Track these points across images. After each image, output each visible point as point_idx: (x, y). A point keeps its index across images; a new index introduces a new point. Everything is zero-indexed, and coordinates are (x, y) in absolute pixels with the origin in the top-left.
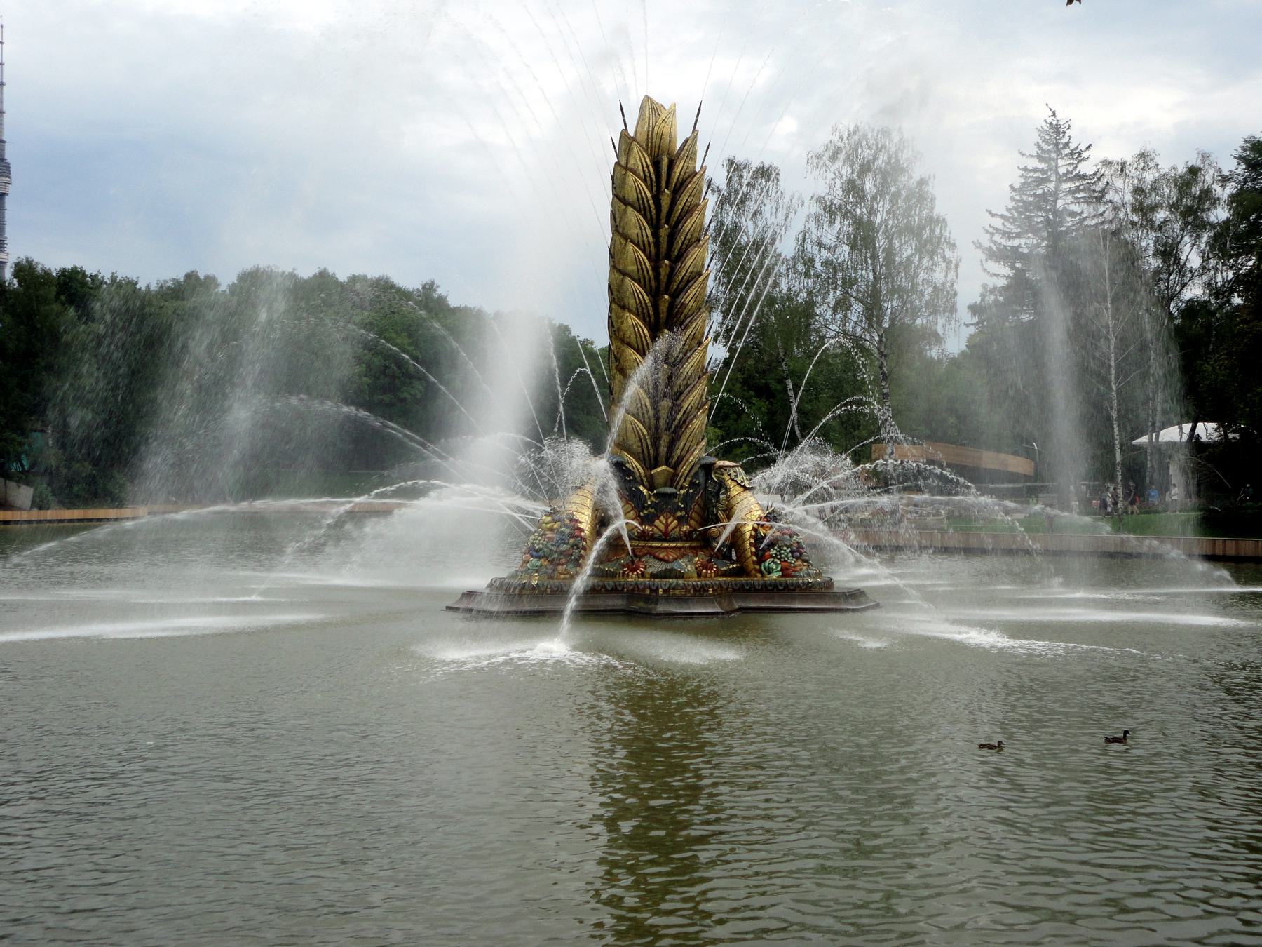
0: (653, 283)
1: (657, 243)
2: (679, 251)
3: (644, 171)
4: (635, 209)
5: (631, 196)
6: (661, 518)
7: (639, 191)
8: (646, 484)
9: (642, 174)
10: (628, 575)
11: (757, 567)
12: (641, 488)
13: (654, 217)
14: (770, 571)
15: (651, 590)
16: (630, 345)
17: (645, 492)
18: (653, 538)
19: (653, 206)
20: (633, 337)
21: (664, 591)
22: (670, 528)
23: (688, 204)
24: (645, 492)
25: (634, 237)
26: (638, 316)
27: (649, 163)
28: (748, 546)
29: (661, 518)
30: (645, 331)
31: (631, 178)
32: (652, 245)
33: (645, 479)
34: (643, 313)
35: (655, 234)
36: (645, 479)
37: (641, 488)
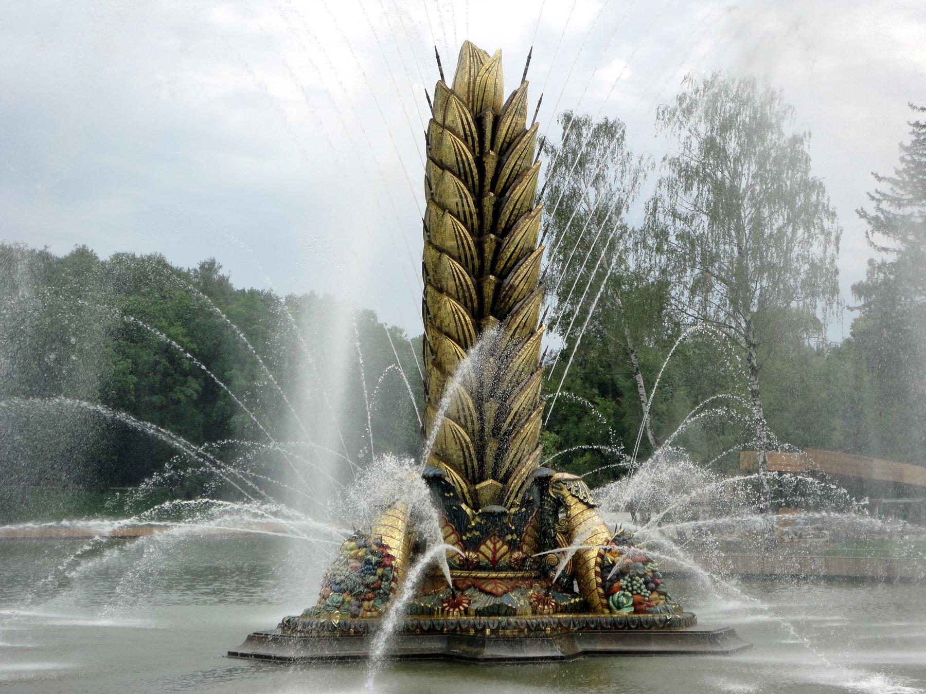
0: (476, 262)
1: (481, 215)
2: (507, 223)
3: (464, 129)
4: (454, 174)
5: (450, 158)
6: (488, 543)
7: (458, 153)
8: (470, 502)
9: (462, 133)
10: (448, 612)
11: (605, 601)
12: (464, 506)
13: (477, 183)
14: (619, 606)
15: (476, 630)
16: (448, 335)
17: (468, 511)
18: (478, 567)
19: (475, 171)
20: (453, 325)
21: (492, 631)
22: (498, 555)
23: (517, 167)
24: (468, 511)
25: (453, 207)
26: (458, 300)
27: (470, 119)
28: (593, 575)
29: (488, 543)
30: (467, 318)
31: (449, 138)
32: (475, 217)
33: (468, 496)
34: (464, 297)
35: (479, 204)
36: (468, 496)
37: (464, 506)
